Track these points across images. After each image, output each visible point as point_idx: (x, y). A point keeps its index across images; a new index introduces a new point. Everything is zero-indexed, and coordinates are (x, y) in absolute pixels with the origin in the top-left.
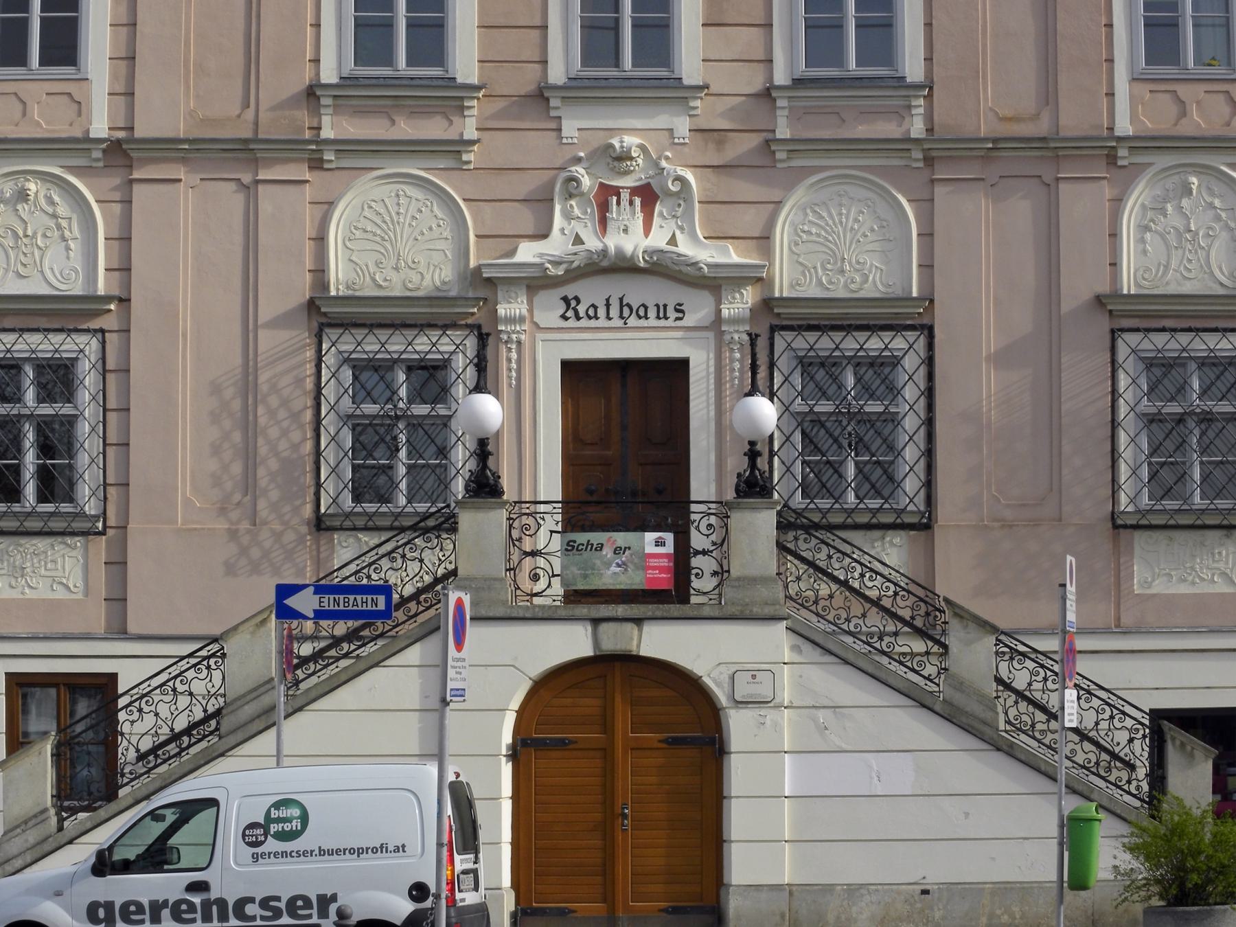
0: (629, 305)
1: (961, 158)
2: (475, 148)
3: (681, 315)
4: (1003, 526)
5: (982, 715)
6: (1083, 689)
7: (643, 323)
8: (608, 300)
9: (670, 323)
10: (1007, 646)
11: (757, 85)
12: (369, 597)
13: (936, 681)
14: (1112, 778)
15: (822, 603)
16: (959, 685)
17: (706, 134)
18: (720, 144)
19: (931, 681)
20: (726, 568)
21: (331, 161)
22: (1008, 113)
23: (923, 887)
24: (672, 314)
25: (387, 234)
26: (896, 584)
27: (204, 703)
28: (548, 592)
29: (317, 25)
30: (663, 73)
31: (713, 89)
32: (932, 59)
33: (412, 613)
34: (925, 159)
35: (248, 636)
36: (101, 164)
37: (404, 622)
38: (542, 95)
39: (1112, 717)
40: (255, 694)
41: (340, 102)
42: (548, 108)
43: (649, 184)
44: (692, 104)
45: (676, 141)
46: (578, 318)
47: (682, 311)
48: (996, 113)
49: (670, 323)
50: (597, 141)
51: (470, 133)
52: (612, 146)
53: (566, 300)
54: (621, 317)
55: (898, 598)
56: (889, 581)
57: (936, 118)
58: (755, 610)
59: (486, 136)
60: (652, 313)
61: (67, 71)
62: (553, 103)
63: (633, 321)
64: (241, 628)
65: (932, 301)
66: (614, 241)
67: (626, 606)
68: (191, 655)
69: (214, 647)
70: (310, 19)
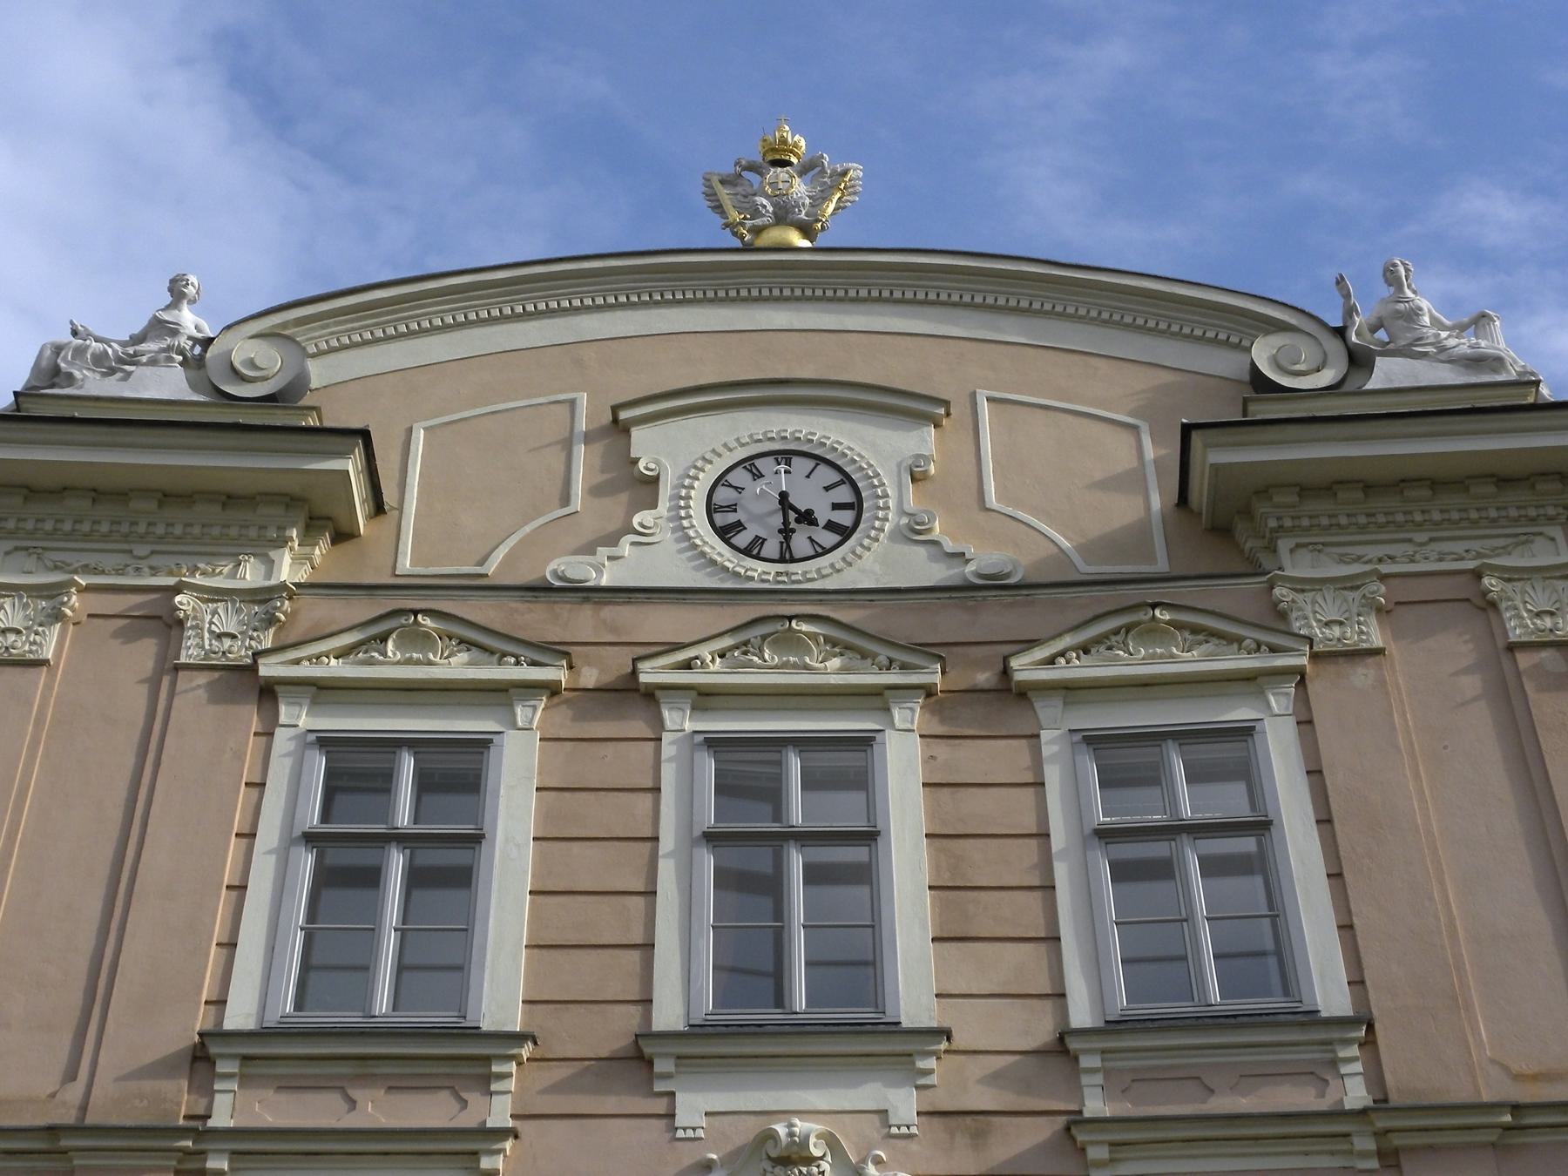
1: (1450, 1148)
2: (508, 1145)
11: (1041, 1031)
17: (953, 1122)
18: (979, 1138)
29: (230, 945)
30: (865, 1014)
31: (959, 1041)
32: (1363, 982)
34: (1381, 1154)
41: (252, 1070)
42: (651, 1076)
44: (922, 1064)
45: (894, 1130)
48: (1506, 1069)
50: (746, 1131)
51: (499, 1114)
52: (772, 1136)
57: (1388, 1077)
59: (524, 1127)
62: (660, 1066)
66: (1292, 595)
70: (218, 932)
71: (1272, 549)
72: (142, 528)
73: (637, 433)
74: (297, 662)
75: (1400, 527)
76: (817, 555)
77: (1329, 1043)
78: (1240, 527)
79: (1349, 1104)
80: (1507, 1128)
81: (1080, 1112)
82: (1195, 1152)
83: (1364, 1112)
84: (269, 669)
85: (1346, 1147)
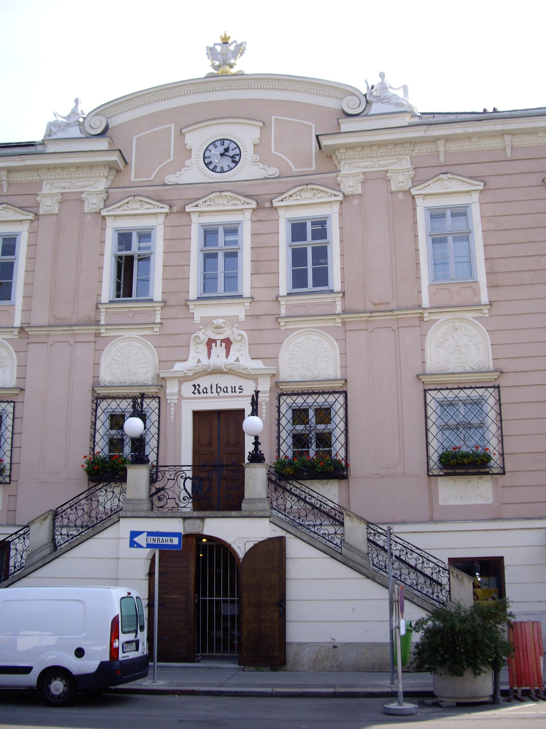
0: (220, 387)
5: (360, 562)
6: (409, 549)
7: (226, 394)
9: (237, 394)
10: (372, 529)
13: (340, 546)
14: (424, 592)
15: (287, 510)
16: (350, 547)
19: (337, 546)
21: (104, 333)
22: (376, 302)
23: (334, 645)
24: (237, 390)
25: (127, 361)
26: (321, 501)
27: (21, 553)
28: (166, 506)
33: (109, 515)
34: (342, 323)
35: (39, 524)
36: (17, 337)
37: (105, 519)
38: (186, 304)
39: (423, 562)
40: (40, 550)
41: (108, 310)
42: (189, 309)
46: (199, 393)
47: (242, 389)
49: (237, 394)
53: (194, 386)
54: (217, 392)
56: (317, 500)
58: (255, 513)
60: (229, 390)
61: (6, 302)
63: (222, 393)
64: (36, 521)
65: (346, 381)
67: (197, 512)
68: (16, 533)
69: (26, 529)
71: (339, 163)
72: (73, 176)
73: (187, 136)
74: (109, 211)
75: (370, 157)
76: (230, 170)
77: (335, 297)
78: (334, 157)
83: (339, 314)
84: (103, 213)
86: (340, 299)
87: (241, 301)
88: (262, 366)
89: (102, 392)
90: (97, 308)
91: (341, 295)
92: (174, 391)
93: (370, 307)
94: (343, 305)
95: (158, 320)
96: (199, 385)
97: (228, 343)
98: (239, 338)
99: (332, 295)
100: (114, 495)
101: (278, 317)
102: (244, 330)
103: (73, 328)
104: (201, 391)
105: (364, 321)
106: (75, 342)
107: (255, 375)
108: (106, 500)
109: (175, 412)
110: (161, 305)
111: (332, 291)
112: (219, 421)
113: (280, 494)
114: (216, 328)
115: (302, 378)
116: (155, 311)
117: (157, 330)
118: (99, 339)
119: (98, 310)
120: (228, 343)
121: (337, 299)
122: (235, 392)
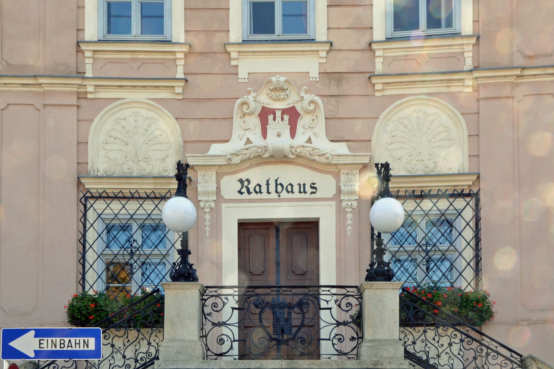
0: (281, 184)
3: (314, 190)
4: (528, 324)
7: (290, 195)
8: (268, 181)
9: (308, 195)
12: (82, 339)
20: (360, 335)
21: (92, 93)
22: (529, 53)
24: (308, 189)
25: (134, 135)
41: (98, 56)
42: (230, 59)
43: (294, 107)
46: (249, 193)
47: (315, 188)
49: (308, 195)
53: (241, 181)
54: (277, 192)
55: (490, 357)
60: (296, 189)
63: (284, 194)
65: (478, 177)
77: (463, 45)
79: (178, 76)
80: (518, 76)
81: (374, 72)
82: (425, 86)
85: (462, 84)
86: (471, 48)
87: (314, 47)
88: (347, 152)
89: (91, 185)
90: (79, 50)
91: (474, 41)
92: (210, 189)
93: (521, 61)
94: (476, 57)
95: (180, 74)
96: (248, 181)
97: (293, 115)
98: (312, 107)
99: (458, 41)
100: (141, 336)
101: (371, 75)
102: (318, 96)
103: (41, 81)
104: (252, 190)
105: (509, 83)
106: (45, 106)
107: (336, 165)
108: (127, 344)
109: (211, 220)
110: (185, 49)
111: (456, 35)
112: (277, 237)
113: (419, 334)
114: (275, 89)
115: (409, 172)
116: (175, 60)
117: (179, 90)
118: (83, 102)
119: (80, 54)
120: (293, 115)
121: (466, 48)
122: (305, 192)
